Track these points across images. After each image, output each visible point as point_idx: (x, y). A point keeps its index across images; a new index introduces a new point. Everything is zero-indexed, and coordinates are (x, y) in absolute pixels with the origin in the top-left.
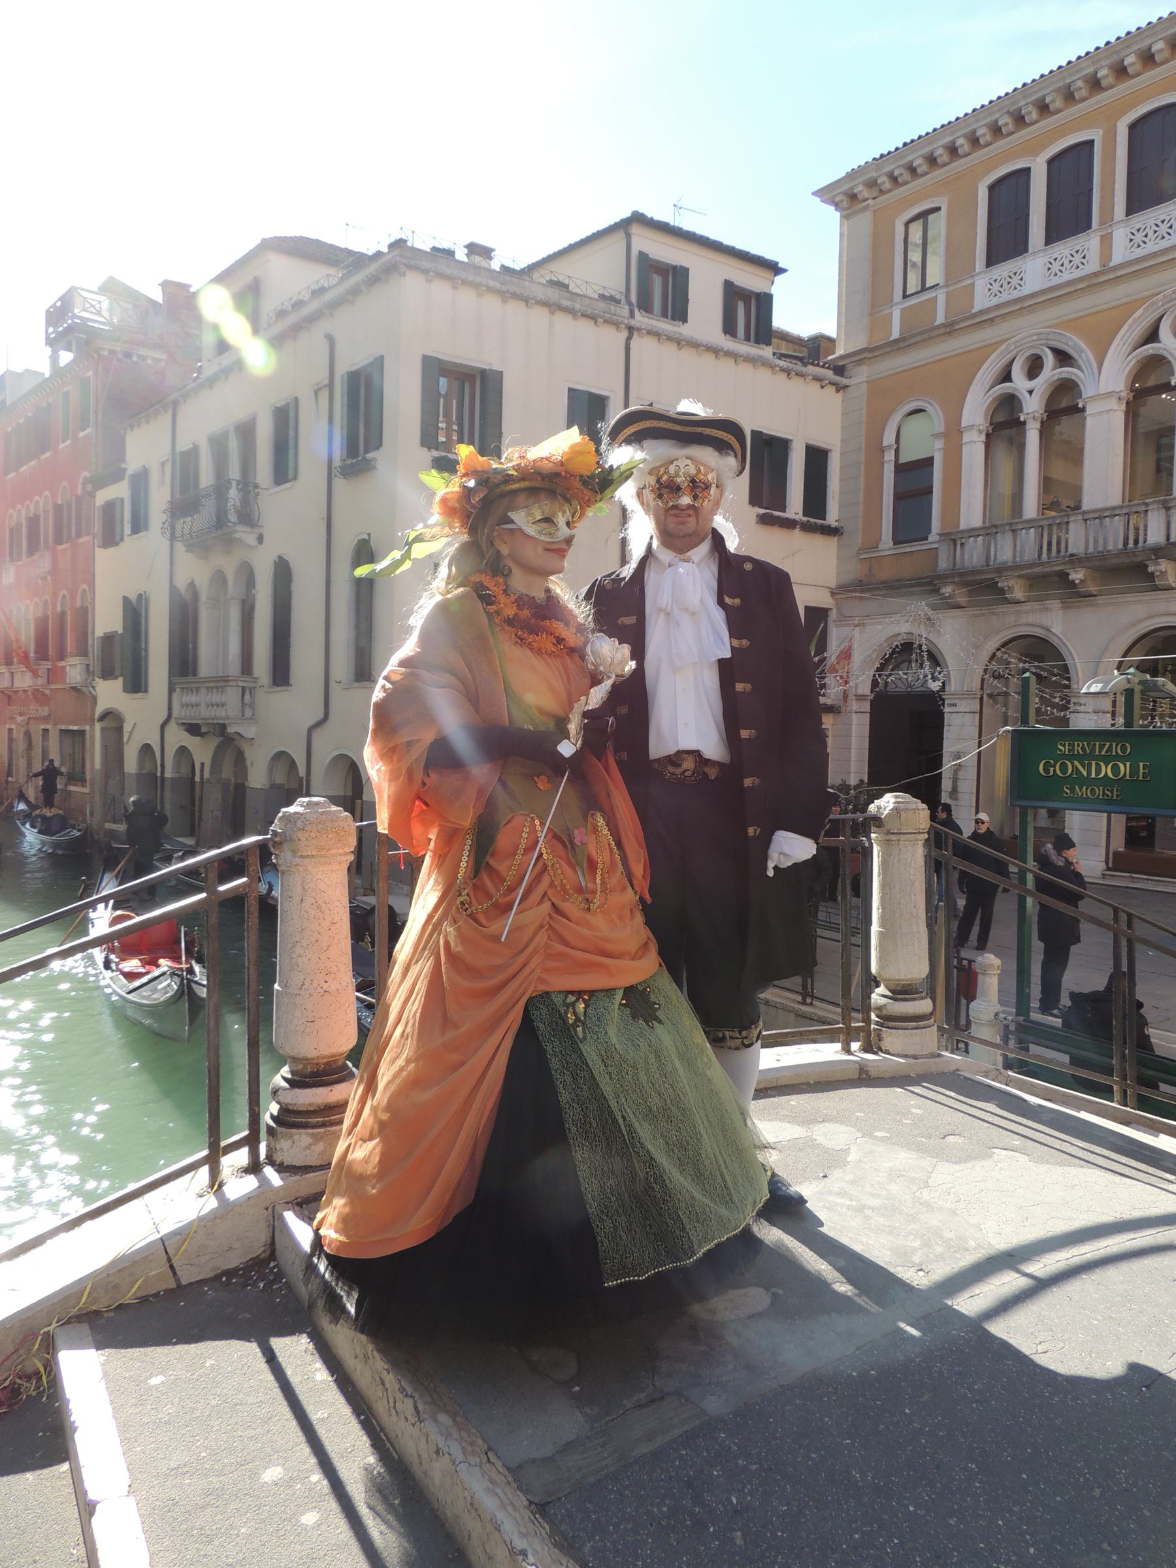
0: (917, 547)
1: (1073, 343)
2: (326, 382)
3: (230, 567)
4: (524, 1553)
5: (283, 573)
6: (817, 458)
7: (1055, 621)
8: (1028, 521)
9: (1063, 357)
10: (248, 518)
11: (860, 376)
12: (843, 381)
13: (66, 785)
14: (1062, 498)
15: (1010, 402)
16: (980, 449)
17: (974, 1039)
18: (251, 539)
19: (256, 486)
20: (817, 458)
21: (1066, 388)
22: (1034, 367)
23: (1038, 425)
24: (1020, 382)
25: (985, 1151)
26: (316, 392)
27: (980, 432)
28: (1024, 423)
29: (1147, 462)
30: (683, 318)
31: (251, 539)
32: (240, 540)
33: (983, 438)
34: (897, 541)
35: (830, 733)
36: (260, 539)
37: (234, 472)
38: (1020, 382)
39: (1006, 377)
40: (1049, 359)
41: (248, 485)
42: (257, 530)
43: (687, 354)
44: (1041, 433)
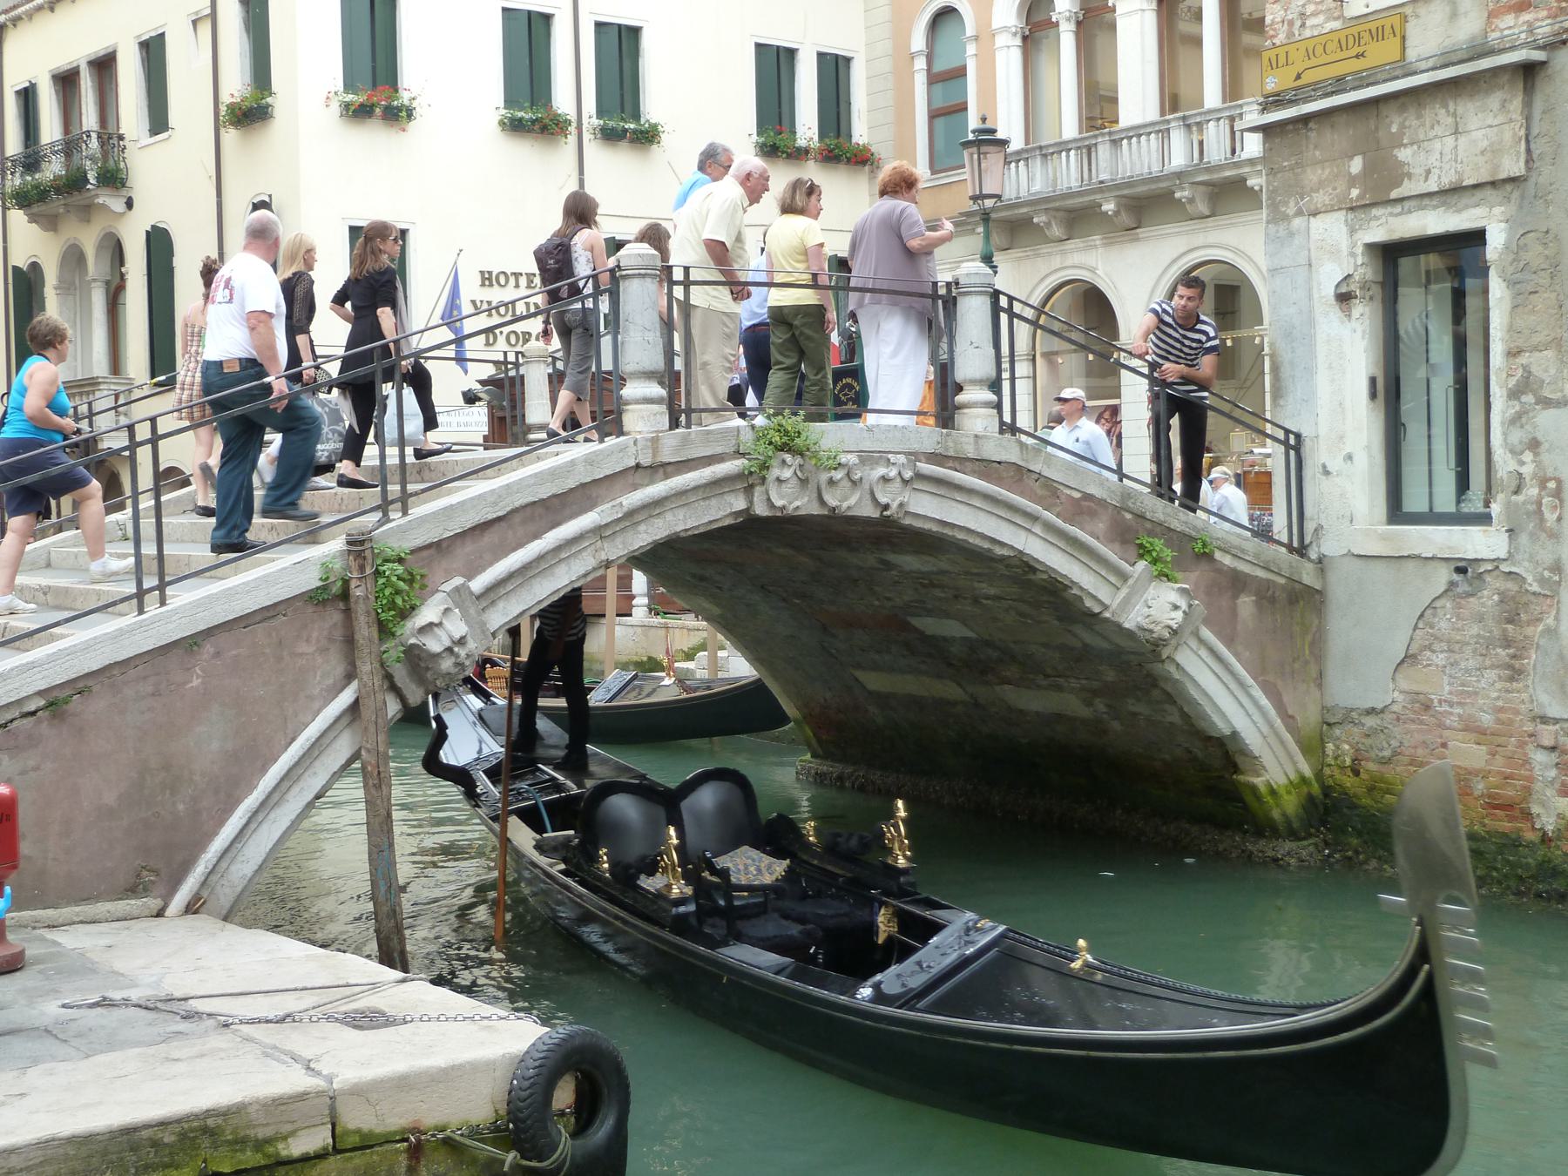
2: (208, 11)
3: (89, 239)
4: (474, 983)
5: (159, 244)
6: (834, 69)
7: (1241, 243)
8: (1210, 111)
10: (113, 179)
14: (1099, 104)
18: (117, 205)
19: (121, 138)
20: (834, 69)
23: (1073, 27)
26: (195, 23)
27: (1015, 34)
28: (1057, 24)
29: (1102, 77)
31: (117, 205)
32: (104, 206)
33: (1018, 41)
36: (129, 204)
37: (1265, 729)
41: (110, 138)
42: (124, 192)
44: (1077, 34)
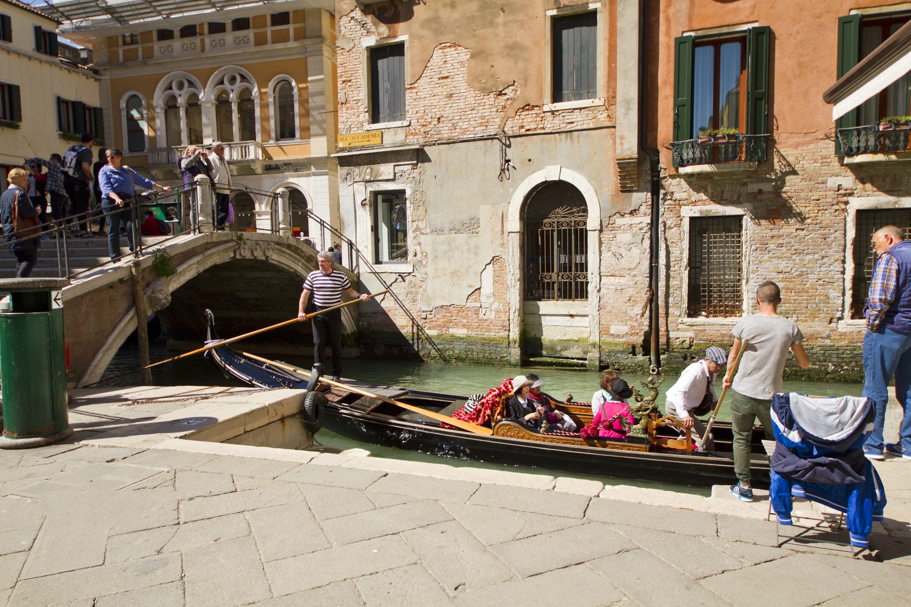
0: (139, 154)
1: (194, 79)
9: (243, 78)
11: (107, 77)
12: (99, 77)
13: (282, 196)
15: (174, 98)
16: (163, 116)
17: (560, 351)
21: (195, 96)
22: (233, 80)
24: (175, 91)
25: (334, 437)
30: (10, 40)
34: (131, 150)
35: (833, 156)
38: (227, 85)
39: (222, 83)
40: (238, 78)
43: (13, 57)
